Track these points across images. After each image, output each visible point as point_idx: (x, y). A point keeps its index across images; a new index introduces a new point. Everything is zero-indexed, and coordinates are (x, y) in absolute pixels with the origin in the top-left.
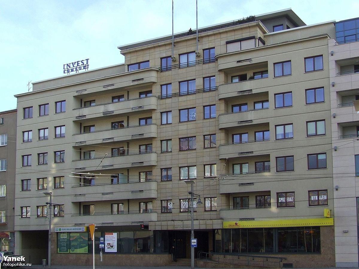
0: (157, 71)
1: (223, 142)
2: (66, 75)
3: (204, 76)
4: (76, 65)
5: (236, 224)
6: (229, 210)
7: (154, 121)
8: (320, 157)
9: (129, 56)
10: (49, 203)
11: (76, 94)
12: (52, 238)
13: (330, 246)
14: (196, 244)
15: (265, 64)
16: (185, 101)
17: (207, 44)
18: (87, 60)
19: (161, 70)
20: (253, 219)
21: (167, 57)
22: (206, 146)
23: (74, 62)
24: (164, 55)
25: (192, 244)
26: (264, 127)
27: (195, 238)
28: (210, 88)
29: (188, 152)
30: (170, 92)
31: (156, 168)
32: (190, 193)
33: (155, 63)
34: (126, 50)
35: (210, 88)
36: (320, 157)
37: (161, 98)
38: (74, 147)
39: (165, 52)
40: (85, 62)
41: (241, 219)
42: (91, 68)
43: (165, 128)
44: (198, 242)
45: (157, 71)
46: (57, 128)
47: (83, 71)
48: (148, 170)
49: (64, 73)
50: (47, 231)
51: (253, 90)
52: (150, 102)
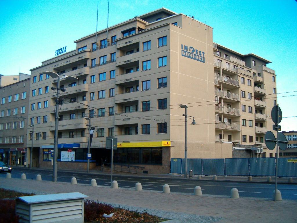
0: (90, 52)
1: (118, 93)
2: (57, 56)
3: (111, 53)
4: (61, 51)
5: (120, 145)
6: (122, 135)
7: (87, 81)
8: (148, 102)
9: (78, 43)
10: (88, 125)
11: (54, 68)
12: (41, 152)
13: (167, 160)
14: (90, 157)
15: (137, 44)
16: (101, 69)
17: (113, 34)
18: (66, 47)
19: (92, 50)
20: (129, 142)
21: (104, 40)
22: (100, 98)
23: (58, 50)
24: (93, 42)
25: (88, 157)
26: (136, 83)
27: (90, 153)
28: (100, 63)
29: (102, 100)
30: (96, 63)
31: (87, 110)
32: (183, 115)
33: (89, 48)
34: (77, 42)
35: (100, 63)
36: (148, 102)
37: (92, 67)
38: (52, 98)
39: (93, 40)
40: (65, 48)
41: (124, 142)
42: (68, 51)
43: (93, 85)
44: (92, 155)
45: (90, 52)
46: (101, 75)
47: (64, 53)
48: (82, 111)
49: (56, 55)
50: (39, 148)
51: (132, 60)
52: (86, 70)
